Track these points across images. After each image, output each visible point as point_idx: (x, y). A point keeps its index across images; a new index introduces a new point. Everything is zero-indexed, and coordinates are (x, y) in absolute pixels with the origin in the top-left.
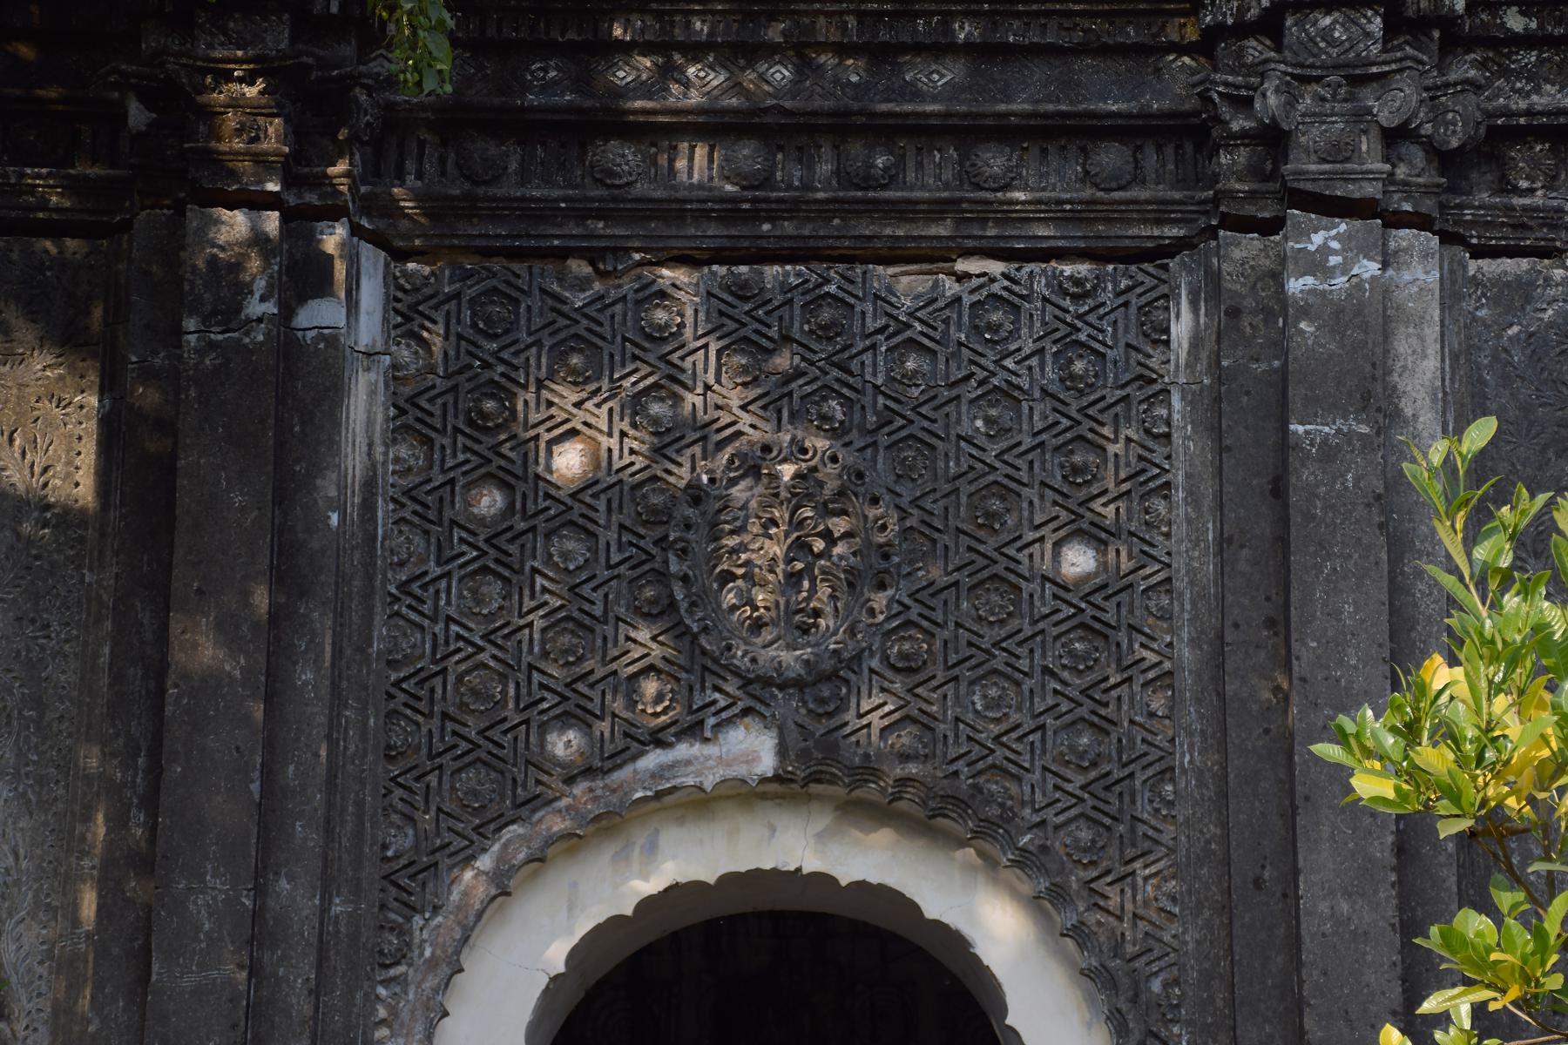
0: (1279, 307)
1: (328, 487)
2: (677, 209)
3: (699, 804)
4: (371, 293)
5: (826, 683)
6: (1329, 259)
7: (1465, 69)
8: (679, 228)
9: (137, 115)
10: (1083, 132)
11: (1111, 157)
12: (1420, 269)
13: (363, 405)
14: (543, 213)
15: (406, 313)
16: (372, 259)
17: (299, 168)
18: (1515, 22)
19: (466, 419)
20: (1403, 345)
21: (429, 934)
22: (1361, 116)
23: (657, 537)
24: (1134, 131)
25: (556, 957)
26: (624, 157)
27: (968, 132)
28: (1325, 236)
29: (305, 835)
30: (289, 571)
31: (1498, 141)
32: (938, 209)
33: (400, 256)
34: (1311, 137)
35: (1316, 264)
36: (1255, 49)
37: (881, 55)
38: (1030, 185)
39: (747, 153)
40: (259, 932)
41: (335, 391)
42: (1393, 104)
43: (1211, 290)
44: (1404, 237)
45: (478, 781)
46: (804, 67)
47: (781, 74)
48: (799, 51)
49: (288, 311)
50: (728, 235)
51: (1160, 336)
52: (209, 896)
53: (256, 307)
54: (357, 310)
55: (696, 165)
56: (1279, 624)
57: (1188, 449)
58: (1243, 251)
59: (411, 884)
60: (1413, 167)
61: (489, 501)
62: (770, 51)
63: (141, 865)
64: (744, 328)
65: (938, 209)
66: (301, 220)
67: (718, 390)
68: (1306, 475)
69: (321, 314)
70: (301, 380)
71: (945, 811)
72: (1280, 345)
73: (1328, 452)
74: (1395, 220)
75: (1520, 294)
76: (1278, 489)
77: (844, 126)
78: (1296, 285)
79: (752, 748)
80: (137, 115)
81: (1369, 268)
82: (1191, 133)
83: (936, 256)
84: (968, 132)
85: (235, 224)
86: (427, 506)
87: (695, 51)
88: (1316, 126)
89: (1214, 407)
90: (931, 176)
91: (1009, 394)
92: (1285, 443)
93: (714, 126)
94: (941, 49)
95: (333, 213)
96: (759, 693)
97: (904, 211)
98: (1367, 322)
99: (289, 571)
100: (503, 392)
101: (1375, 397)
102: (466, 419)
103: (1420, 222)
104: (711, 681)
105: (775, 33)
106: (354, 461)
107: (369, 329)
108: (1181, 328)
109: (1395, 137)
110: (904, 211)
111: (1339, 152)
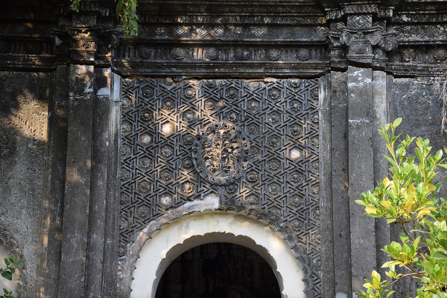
0: (346, 91)
1: (106, 135)
2: (194, 65)
3: (200, 215)
4: (117, 86)
5: (232, 185)
6: (358, 78)
7: (392, 30)
8: (194, 70)
9: (58, 41)
10: (295, 46)
11: (304, 52)
12: (381, 80)
13: (115, 115)
14: (161, 66)
15: (126, 91)
16: (117, 78)
17: (98, 55)
18: (405, 19)
19: (140, 118)
20: (377, 100)
21: (131, 248)
22: (366, 42)
23: (189, 149)
24: (309, 46)
25: (163, 254)
26: (180, 52)
27: (267, 46)
28: (357, 72)
29: (100, 223)
30: (96, 157)
31: (401, 48)
32: (260, 65)
33: (124, 77)
34: (354, 47)
35: (355, 80)
36: (340, 25)
37: (246, 26)
38: (284, 59)
39: (212, 51)
40: (89, 247)
41: (107, 111)
42: (374, 40)
43: (329, 85)
44: (377, 73)
45: (142, 208)
46: (226, 29)
47: (220, 31)
48: (225, 25)
49: (96, 91)
50: (208, 71)
51: (316, 98)
52: (76, 239)
53: (88, 90)
54: (113, 91)
55: (199, 54)
56: (346, 170)
57: (323, 127)
58: (337, 76)
59: (126, 236)
60: (380, 55)
61: (147, 139)
62: (217, 25)
63: (59, 231)
64: (211, 95)
65: (260, 65)
66: (99, 68)
67: (204, 111)
68: (352, 133)
69: (104, 92)
70: (99, 108)
71: (261, 217)
72: (346, 100)
73: (358, 127)
74: (375, 69)
75: (407, 87)
76: (346, 136)
77: (236, 44)
78: (350, 85)
79: (213, 202)
80: (58, 41)
81: (369, 81)
82: (324, 46)
83: (259, 77)
84: (267, 46)
85: (82, 69)
86: (131, 140)
87: (199, 25)
88: (355, 46)
89: (330, 115)
90: (258, 57)
91: (278, 112)
92: (347, 125)
93: (204, 44)
94: (260, 25)
95: (107, 66)
96: (215, 187)
97: (251, 66)
98: (368, 94)
99: (96, 157)
100: (150, 112)
101: (370, 113)
102: (140, 118)
103: (381, 69)
104: (203, 184)
105: (219, 21)
106: (112, 129)
107: (116, 95)
108: (322, 95)
109: (375, 48)
110: (251, 66)
111: (361, 51)
